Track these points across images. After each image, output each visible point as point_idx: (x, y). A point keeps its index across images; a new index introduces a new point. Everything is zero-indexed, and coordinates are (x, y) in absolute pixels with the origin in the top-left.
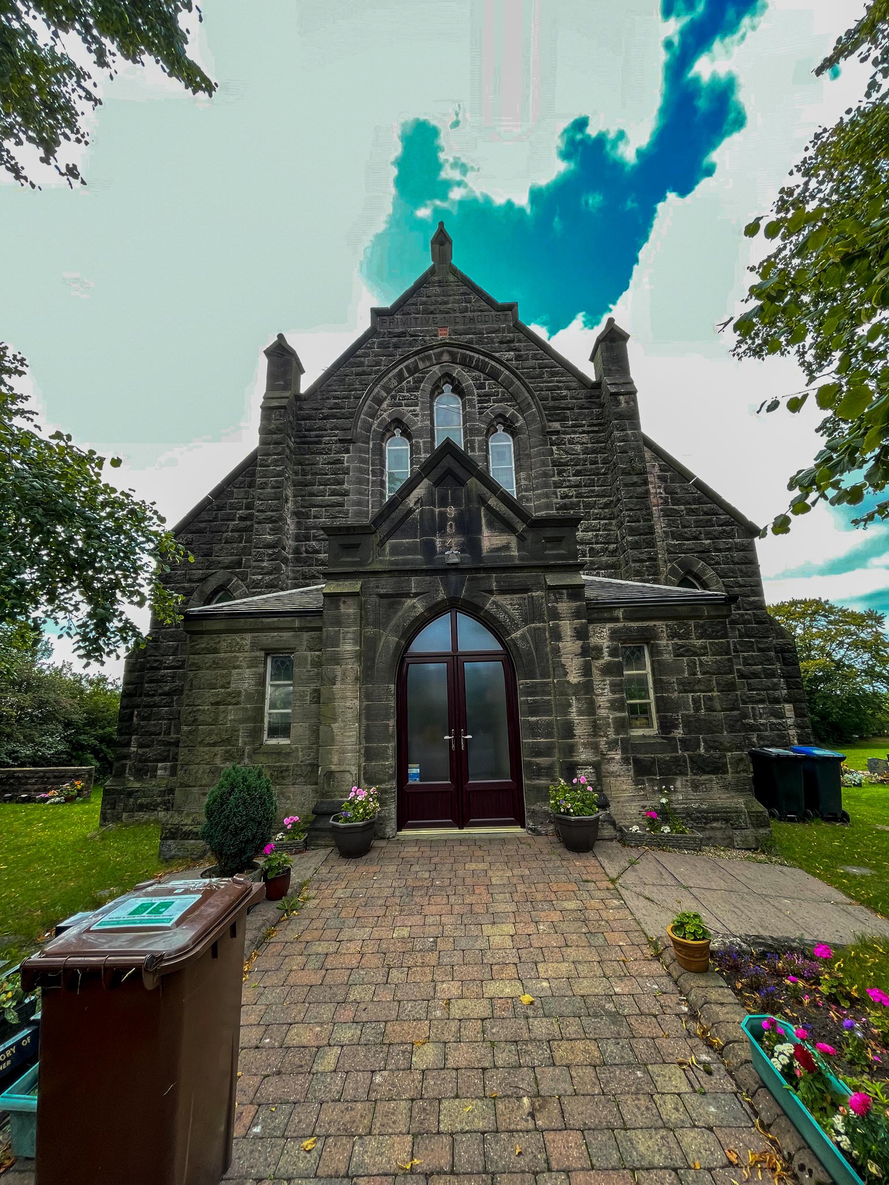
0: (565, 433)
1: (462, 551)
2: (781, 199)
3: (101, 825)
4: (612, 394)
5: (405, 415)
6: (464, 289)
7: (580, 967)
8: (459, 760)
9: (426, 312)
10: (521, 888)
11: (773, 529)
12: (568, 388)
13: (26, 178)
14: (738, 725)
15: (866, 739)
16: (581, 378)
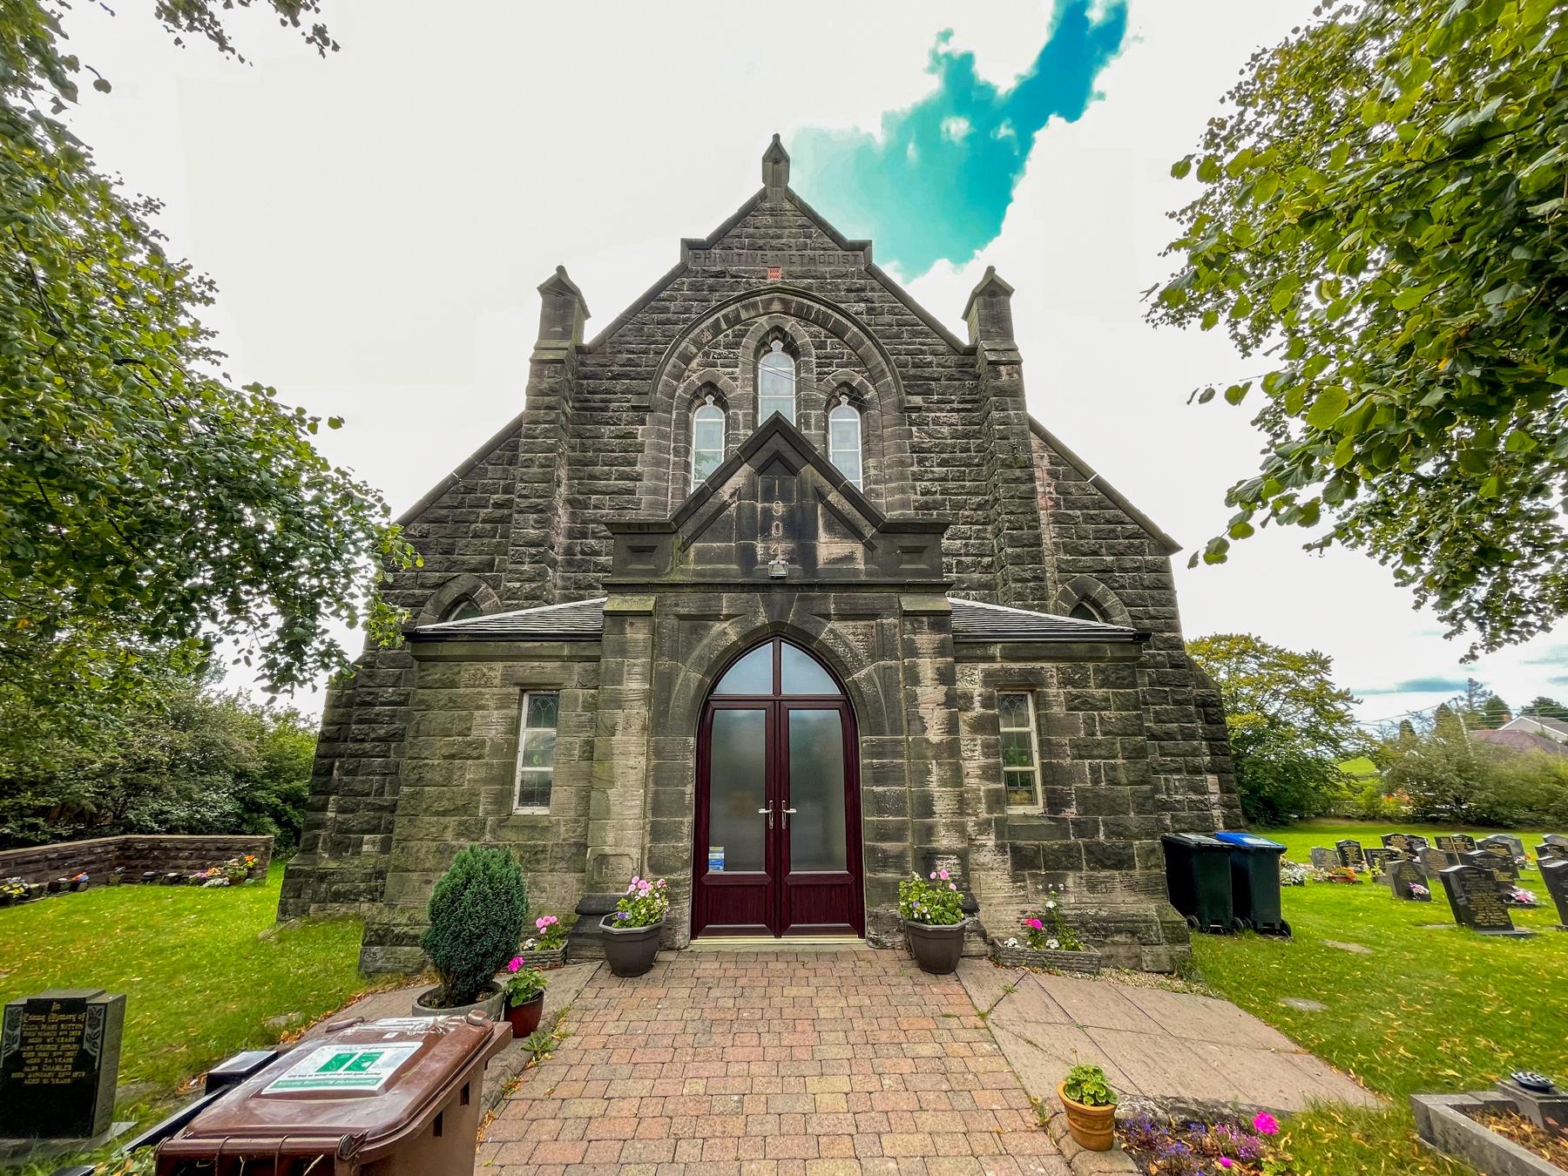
0: (928, 410)
1: (791, 561)
2: (1211, 132)
3: (279, 920)
4: (990, 363)
5: (719, 378)
6: (803, 220)
7: (939, 1141)
8: (778, 842)
9: (753, 247)
10: (859, 1024)
11: (1205, 557)
12: (934, 353)
13: (233, 51)
14: (1150, 805)
15: (1308, 820)
16: (951, 342)
